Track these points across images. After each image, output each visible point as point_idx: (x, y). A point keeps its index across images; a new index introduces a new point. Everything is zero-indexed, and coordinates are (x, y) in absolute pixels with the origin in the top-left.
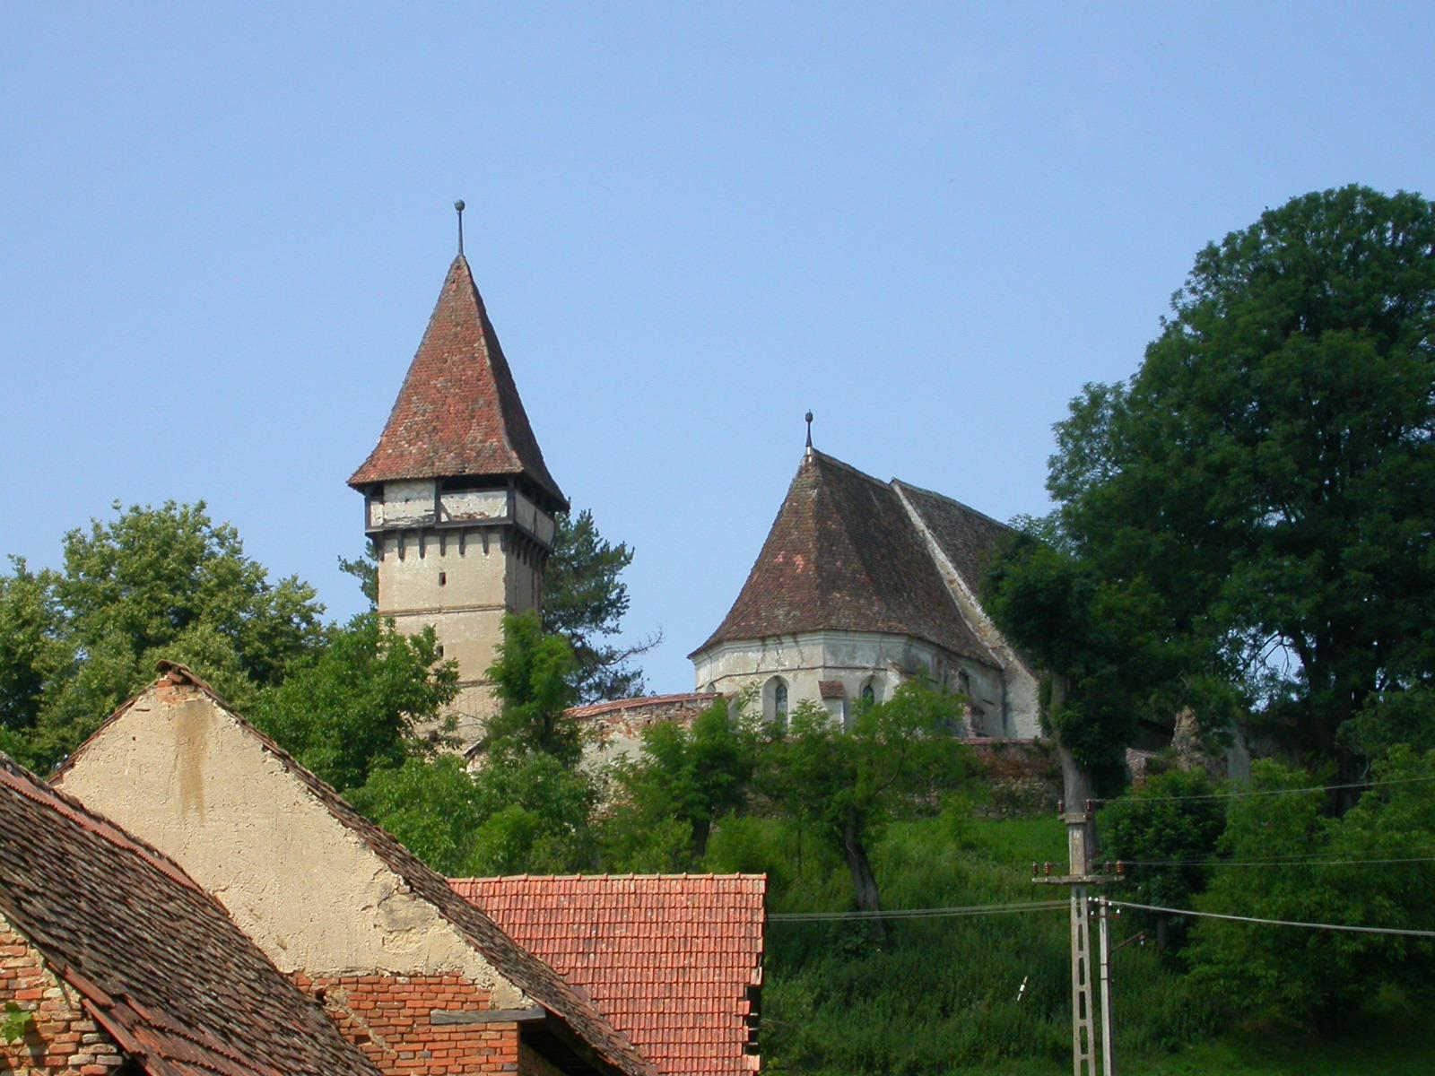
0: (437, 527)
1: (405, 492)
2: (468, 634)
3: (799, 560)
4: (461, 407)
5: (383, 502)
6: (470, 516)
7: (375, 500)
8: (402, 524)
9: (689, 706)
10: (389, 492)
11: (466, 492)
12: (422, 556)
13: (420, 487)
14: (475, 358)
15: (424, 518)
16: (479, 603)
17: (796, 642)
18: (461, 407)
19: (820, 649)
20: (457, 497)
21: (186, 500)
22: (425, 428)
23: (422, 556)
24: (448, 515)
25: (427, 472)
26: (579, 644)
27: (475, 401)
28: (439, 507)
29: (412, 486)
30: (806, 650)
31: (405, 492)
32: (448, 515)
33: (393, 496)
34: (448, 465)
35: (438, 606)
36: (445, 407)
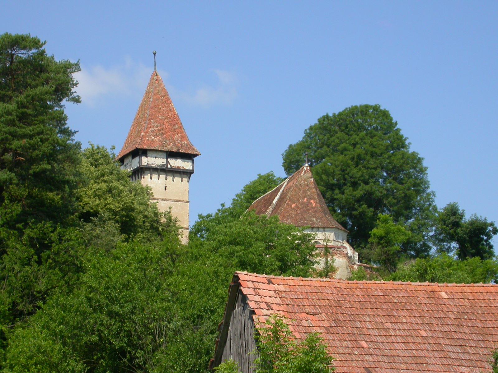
0: (166, 169)
1: (155, 155)
2: (176, 209)
3: (312, 202)
4: (170, 127)
5: (147, 157)
6: (178, 167)
7: (144, 156)
8: (154, 166)
9: (338, 250)
10: (149, 153)
11: (177, 158)
12: (159, 179)
13: (160, 154)
14: (171, 110)
15: (162, 165)
16: (179, 199)
17: (324, 230)
18: (170, 127)
19: (333, 234)
20: (174, 160)
21: (286, 147)
22: (159, 132)
23: (159, 179)
24: (170, 165)
25: (165, 149)
26: (361, 221)
27: (175, 125)
28: (168, 162)
29: (158, 153)
30: (327, 233)
31: (155, 154)
32: (170, 165)
33: (150, 155)
34: (171, 147)
35: (165, 198)
36: (164, 126)
